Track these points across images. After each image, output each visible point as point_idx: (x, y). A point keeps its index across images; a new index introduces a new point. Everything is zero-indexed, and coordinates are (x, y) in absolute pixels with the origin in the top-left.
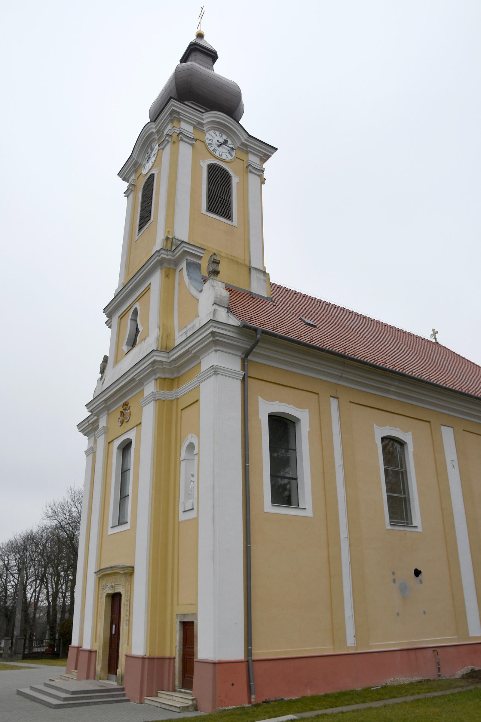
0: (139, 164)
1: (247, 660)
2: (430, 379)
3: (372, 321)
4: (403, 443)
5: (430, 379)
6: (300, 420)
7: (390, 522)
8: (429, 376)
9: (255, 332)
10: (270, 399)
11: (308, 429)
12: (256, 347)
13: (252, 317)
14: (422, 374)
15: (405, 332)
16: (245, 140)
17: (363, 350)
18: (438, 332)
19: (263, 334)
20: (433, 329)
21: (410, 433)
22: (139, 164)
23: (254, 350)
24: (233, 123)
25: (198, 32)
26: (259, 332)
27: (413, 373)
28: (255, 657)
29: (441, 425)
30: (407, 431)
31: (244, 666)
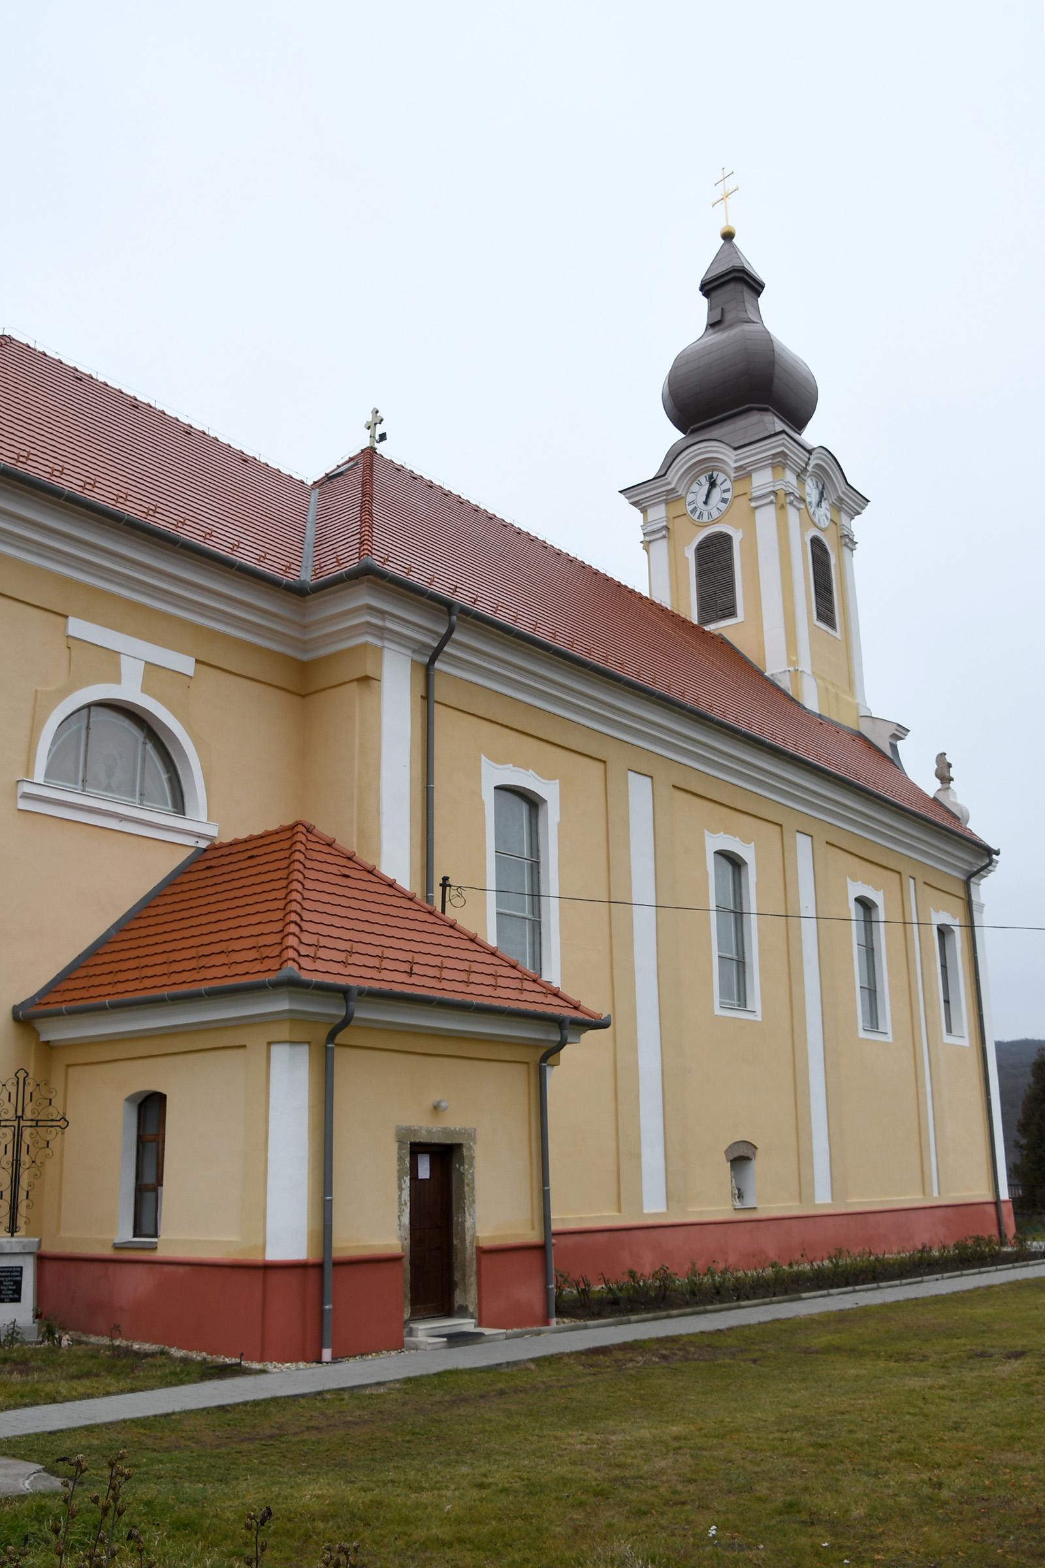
0: (675, 495)
1: (994, 1201)
2: (518, 620)
3: (505, 526)
4: (740, 863)
5: (518, 620)
6: (746, 863)
7: (721, 1003)
8: (515, 615)
9: (446, 609)
10: (499, 759)
11: (755, 880)
12: (449, 643)
13: (458, 589)
14: (576, 642)
15: (534, 540)
16: (844, 493)
17: (395, 553)
18: (382, 420)
19: (461, 615)
20: (375, 408)
21: (882, 891)
22: (675, 495)
23: (446, 649)
24: (829, 462)
25: (723, 232)
26: (456, 610)
27: (575, 645)
28: (555, 1227)
29: (798, 831)
30: (550, 778)
31: (991, 1209)
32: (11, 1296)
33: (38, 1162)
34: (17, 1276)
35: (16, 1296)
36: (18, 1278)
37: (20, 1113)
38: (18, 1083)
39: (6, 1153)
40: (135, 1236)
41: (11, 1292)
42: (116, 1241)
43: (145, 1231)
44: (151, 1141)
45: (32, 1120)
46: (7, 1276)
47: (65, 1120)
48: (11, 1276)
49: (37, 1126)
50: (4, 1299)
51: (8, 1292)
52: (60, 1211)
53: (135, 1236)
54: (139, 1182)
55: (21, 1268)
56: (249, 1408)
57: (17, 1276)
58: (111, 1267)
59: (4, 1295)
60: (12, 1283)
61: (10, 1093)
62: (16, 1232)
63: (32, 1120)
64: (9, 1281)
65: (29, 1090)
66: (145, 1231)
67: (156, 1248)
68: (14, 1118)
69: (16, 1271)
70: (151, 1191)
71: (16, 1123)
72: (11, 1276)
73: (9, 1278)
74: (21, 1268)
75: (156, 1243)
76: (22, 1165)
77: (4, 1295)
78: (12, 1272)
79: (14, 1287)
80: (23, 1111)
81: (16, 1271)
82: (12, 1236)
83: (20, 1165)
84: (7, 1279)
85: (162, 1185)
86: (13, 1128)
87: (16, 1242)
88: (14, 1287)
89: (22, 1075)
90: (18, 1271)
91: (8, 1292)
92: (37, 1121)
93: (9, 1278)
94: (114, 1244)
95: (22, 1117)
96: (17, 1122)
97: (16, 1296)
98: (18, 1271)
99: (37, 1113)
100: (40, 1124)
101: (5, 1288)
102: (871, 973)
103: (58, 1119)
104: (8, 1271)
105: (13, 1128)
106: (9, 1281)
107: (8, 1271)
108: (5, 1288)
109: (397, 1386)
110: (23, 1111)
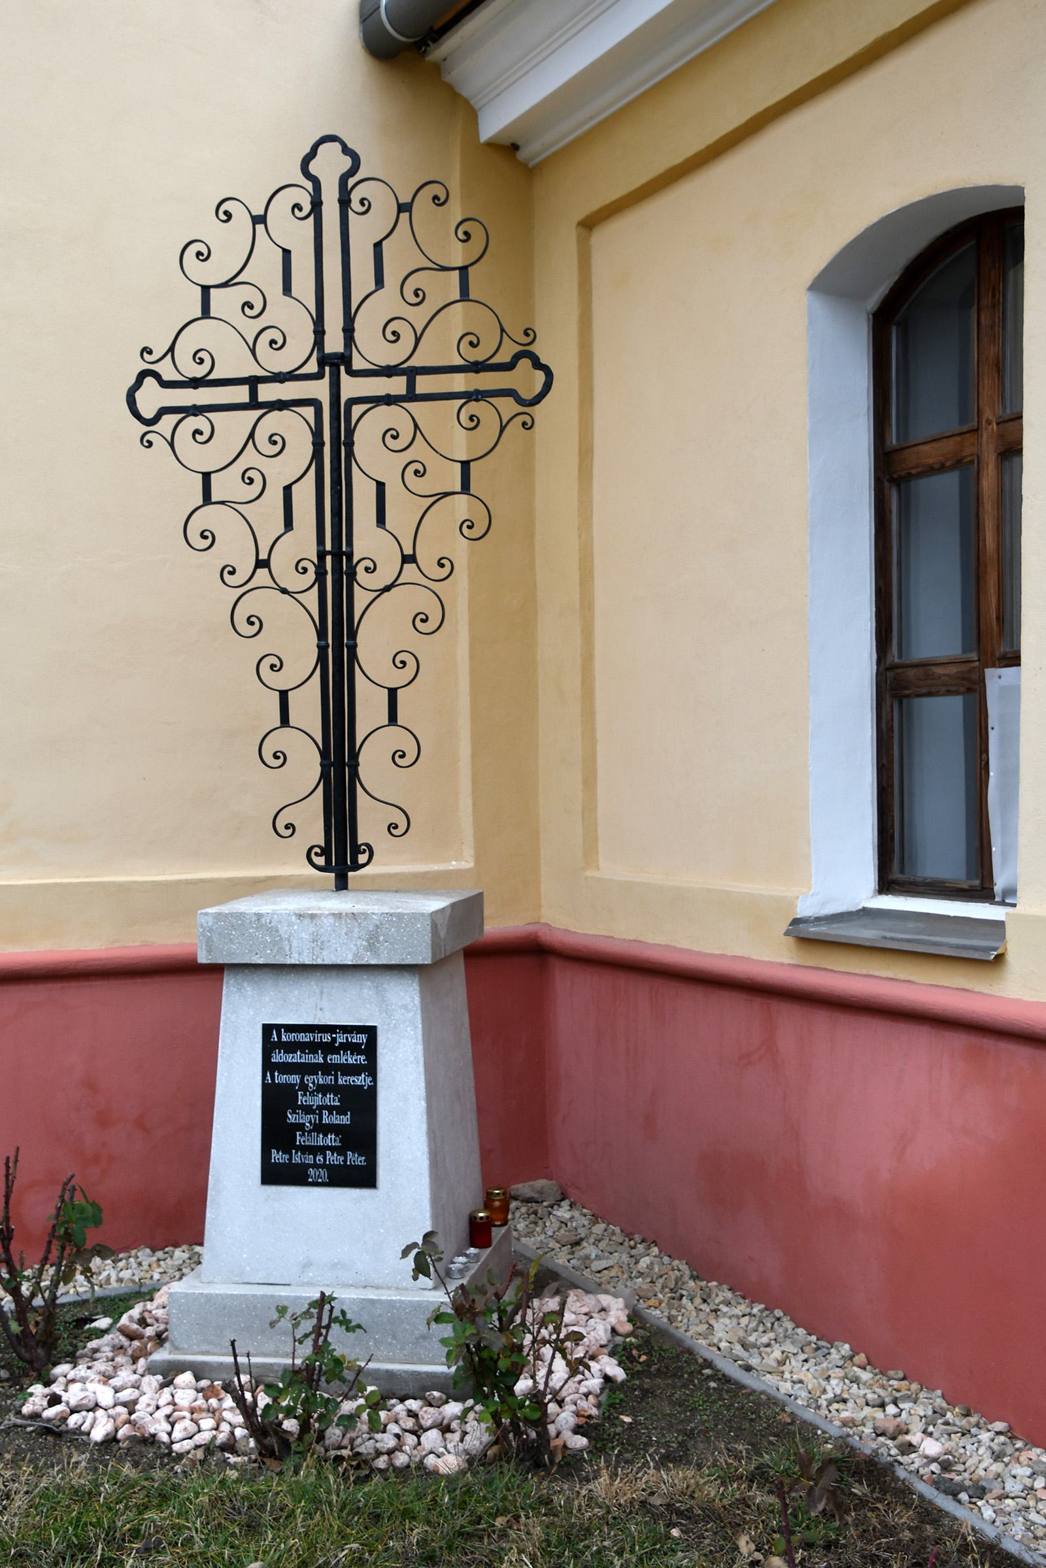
32: (333, 1158)
33: (426, 557)
34: (354, 1070)
35: (355, 1159)
36: (361, 1080)
37: (334, 343)
38: (317, 204)
39: (289, 524)
40: (885, 885)
41: (331, 1140)
42: (805, 909)
43: (931, 868)
44: (942, 468)
45: (388, 371)
46: (312, 1069)
47: (537, 364)
48: (326, 1069)
49: (411, 396)
50: (305, 1167)
51: (320, 1140)
52: (589, 781)
53: (885, 885)
54: (894, 656)
55: (371, 1032)
56: (944, 689)
57: (354, 1070)
58: (789, 1018)
59: (305, 1149)
60: (331, 1100)
61: (287, 253)
62: (357, 866)
63: (388, 371)
64: (323, 1089)
65: (364, 231)
66: (931, 868)
67: (1000, 958)
68: (312, 367)
69: (348, 1047)
70: (949, 693)
71: (320, 390)
72: (326, 1069)
73: (321, 1080)
74: (371, 1032)
75: (1000, 925)
76: (361, 575)
77: (305, 1149)
78: (329, 1048)
79: (345, 1120)
80: (349, 331)
81: (348, 1047)
82: (342, 884)
83: (352, 575)
84: (309, 1080)
85: (1014, 660)
86: (309, 412)
87: (338, 916)
88: (345, 1120)
89: (330, 165)
90: (354, 1048)
91: (320, 1140)
92: (412, 374)
93: (321, 1080)
94: (796, 922)
95: (344, 359)
96: (345, 395)
97: (355, 1159)
98: (354, 1048)
99: (408, 339)
100: (424, 384)
101: (306, 1120)
102: (983, 724)
103: (504, 357)
104: (312, 1047)
105: (309, 412)
106: (323, 1089)
107: (312, 1047)
108: (306, 1120)
109: (907, 692)
110: (349, 331)
